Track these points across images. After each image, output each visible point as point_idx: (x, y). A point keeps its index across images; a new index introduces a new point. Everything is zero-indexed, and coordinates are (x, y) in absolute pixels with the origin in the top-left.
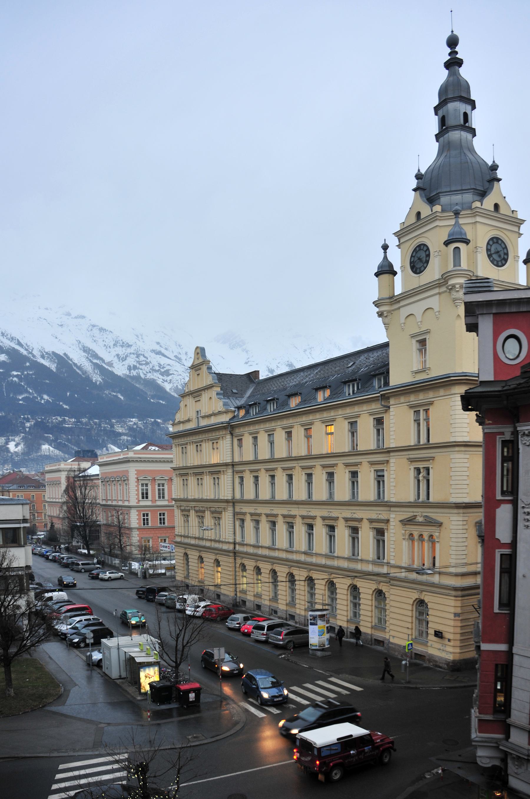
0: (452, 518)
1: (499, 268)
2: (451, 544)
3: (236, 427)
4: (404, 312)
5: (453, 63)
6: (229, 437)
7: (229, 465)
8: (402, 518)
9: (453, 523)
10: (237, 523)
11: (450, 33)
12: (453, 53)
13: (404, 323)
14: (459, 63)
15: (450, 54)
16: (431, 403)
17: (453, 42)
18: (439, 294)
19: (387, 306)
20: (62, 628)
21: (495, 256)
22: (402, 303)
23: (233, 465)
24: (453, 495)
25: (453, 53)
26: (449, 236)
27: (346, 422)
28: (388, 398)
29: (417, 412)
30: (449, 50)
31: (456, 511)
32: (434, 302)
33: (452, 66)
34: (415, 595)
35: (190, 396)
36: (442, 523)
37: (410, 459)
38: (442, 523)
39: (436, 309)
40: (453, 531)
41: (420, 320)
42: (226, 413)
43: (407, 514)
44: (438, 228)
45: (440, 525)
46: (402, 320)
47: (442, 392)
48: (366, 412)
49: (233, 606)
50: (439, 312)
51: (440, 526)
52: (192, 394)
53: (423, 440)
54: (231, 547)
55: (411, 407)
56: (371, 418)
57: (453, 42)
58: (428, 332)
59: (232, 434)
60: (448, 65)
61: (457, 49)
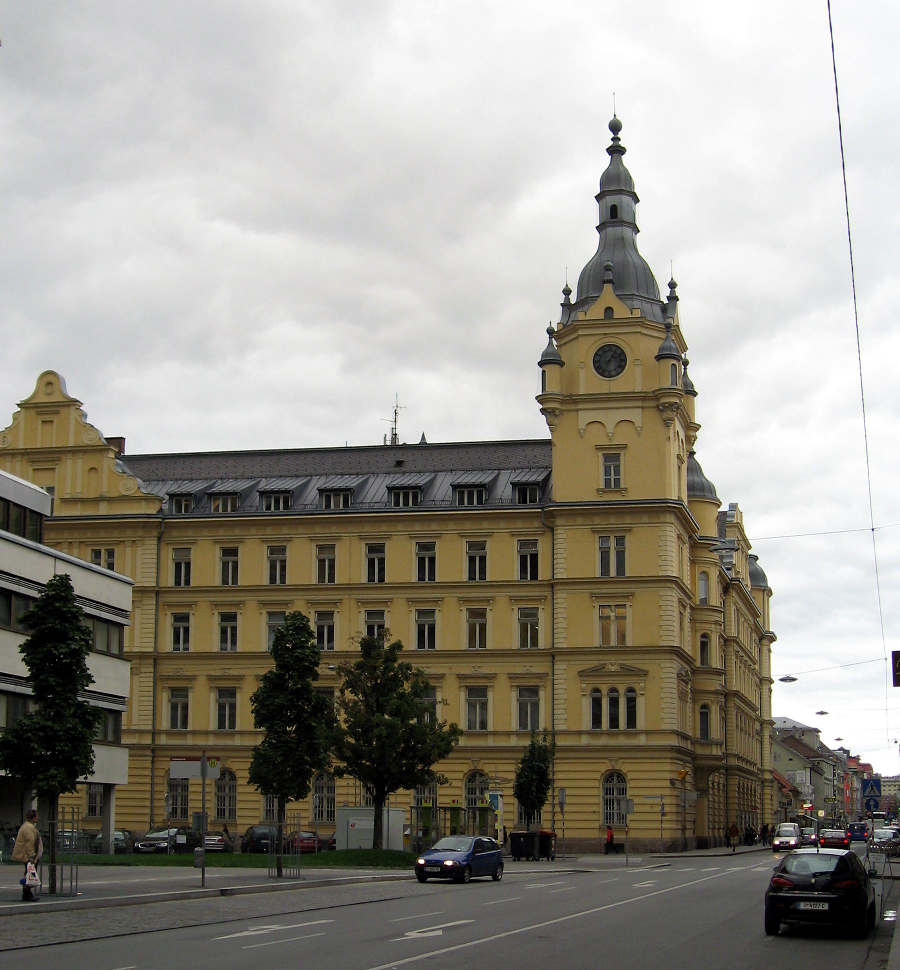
4: (585, 417)
5: (616, 151)
6: (152, 544)
7: (151, 591)
10: (165, 698)
12: (616, 139)
13: (585, 430)
14: (623, 151)
15: (613, 139)
16: (630, 530)
17: (615, 127)
18: (643, 408)
19: (552, 405)
22: (581, 406)
23: (158, 593)
25: (616, 139)
27: (314, 545)
30: (612, 136)
32: (636, 415)
34: (604, 767)
35: (26, 457)
37: (592, 593)
39: (639, 423)
42: (145, 499)
43: (591, 662)
44: (639, 335)
45: (645, 673)
46: (582, 426)
47: (645, 519)
50: (642, 428)
52: (28, 454)
54: (148, 740)
56: (516, 539)
57: (615, 127)
58: (624, 447)
59: (159, 539)
61: (620, 135)
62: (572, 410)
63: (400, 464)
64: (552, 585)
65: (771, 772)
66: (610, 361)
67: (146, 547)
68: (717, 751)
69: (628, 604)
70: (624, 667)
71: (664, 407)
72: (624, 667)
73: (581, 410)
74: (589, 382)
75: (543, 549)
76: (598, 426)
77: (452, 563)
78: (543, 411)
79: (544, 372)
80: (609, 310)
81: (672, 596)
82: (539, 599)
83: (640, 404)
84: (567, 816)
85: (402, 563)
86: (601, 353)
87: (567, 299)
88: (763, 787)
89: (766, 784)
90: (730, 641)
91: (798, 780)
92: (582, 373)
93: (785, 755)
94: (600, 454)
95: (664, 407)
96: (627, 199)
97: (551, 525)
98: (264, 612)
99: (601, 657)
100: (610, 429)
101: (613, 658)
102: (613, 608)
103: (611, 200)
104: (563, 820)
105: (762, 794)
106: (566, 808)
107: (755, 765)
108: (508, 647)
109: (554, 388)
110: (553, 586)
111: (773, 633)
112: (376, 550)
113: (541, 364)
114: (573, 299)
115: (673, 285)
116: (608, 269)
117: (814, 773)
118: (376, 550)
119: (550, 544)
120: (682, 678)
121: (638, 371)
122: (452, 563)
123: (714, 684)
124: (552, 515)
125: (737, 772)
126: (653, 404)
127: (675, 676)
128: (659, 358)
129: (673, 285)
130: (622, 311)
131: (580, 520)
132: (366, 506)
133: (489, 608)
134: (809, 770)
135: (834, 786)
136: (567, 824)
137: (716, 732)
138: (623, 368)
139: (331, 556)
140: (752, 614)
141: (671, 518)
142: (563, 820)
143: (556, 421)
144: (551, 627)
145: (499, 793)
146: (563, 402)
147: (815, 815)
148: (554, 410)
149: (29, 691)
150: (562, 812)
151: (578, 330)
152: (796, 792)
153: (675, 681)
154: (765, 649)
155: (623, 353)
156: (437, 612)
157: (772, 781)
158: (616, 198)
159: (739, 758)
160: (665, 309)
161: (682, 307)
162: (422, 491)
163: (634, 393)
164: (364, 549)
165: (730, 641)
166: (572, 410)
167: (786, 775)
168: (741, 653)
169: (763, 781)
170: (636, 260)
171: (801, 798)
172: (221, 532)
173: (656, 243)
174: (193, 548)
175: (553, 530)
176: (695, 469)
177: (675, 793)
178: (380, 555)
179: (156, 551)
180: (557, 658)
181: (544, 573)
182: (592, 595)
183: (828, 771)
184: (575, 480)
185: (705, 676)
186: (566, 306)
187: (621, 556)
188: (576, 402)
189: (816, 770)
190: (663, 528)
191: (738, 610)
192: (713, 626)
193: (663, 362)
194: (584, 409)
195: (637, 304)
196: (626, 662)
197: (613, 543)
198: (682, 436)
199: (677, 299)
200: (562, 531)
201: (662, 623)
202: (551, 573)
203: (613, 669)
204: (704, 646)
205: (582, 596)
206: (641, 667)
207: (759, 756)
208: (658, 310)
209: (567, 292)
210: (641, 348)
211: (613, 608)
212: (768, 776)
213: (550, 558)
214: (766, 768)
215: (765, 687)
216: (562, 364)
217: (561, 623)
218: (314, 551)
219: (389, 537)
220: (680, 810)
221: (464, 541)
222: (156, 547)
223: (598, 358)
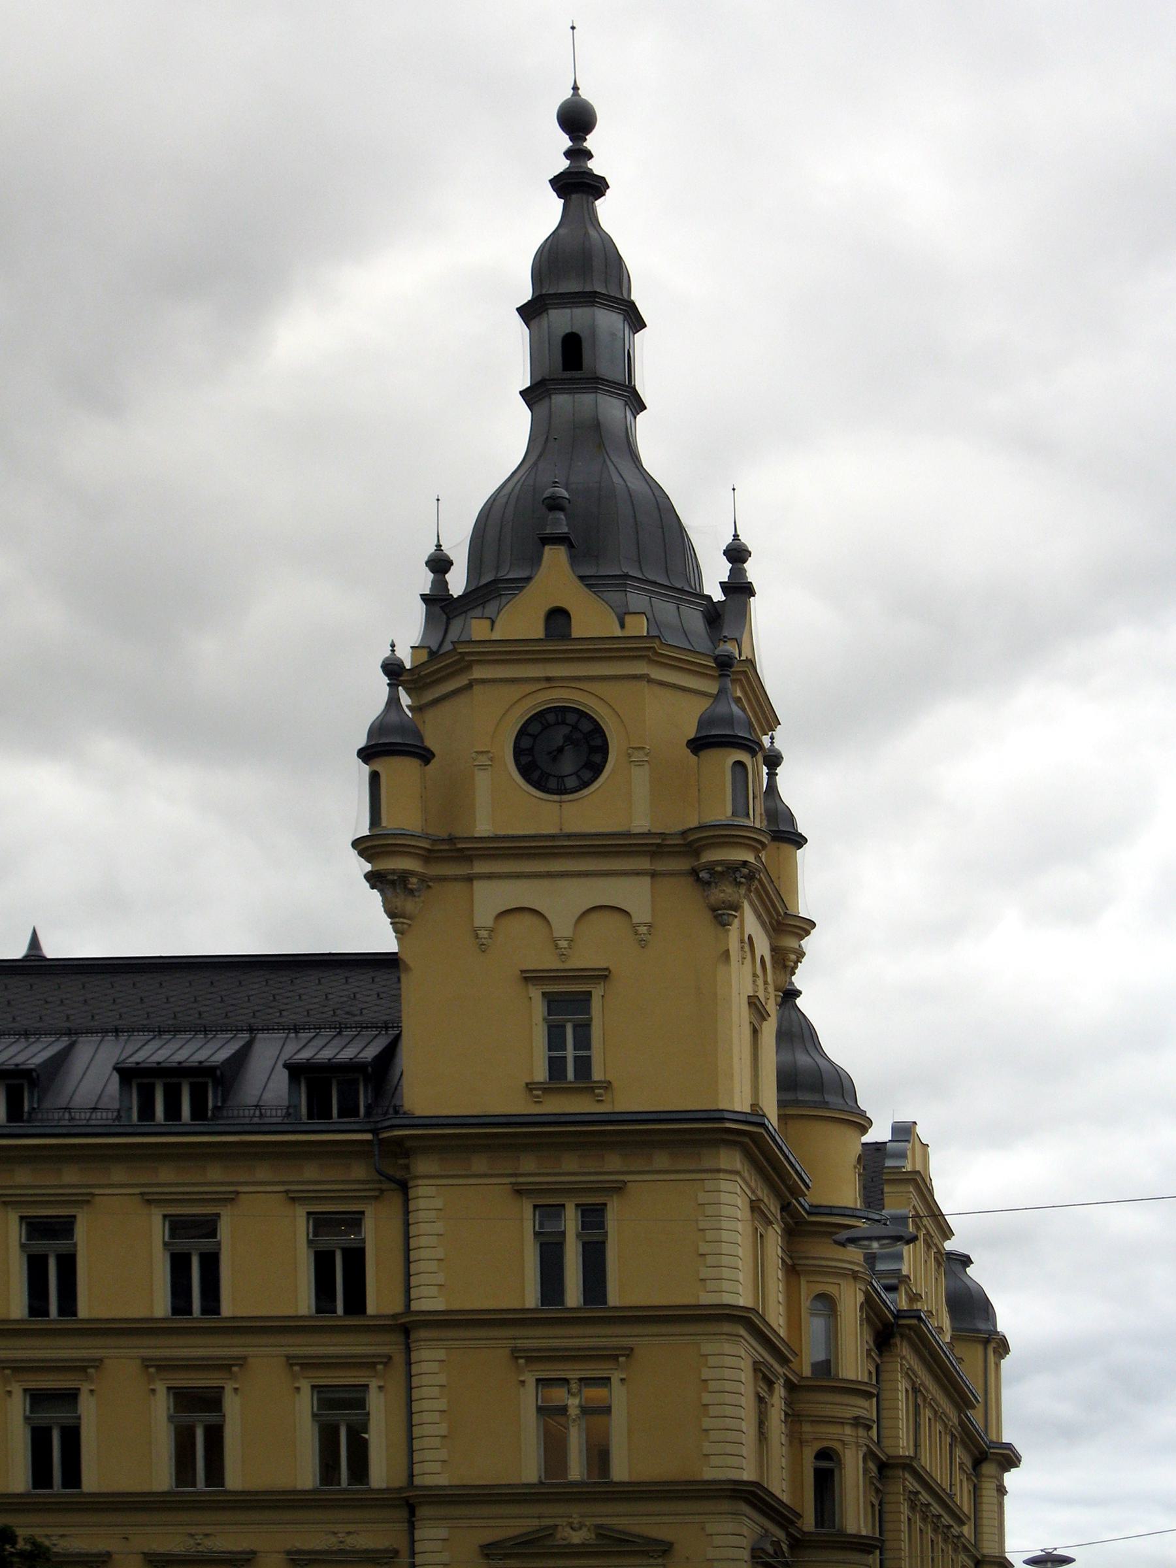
0: (710, 1528)
1: (596, 785)
4: (490, 897)
5: (579, 186)
8: (488, 1536)
9: (717, 1540)
11: (568, 94)
12: (578, 154)
13: (491, 930)
14: (598, 187)
15: (568, 154)
16: (619, 1189)
17: (577, 120)
18: (654, 875)
21: (483, 723)
22: (480, 867)
24: (715, 1461)
25: (578, 154)
26: (701, 724)
28: (407, 1154)
29: (549, 1212)
30: (566, 142)
31: (726, 1506)
32: (634, 894)
33: (583, 192)
36: (671, 1545)
38: (671, 1545)
39: (641, 912)
41: (568, 933)
46: (484, 917)
47: (662, 1160)
48: (137, 1191)
50: (650, 926)
51: (665, 1552)
55: (520, 1192)
57: (577, 120)
58: (602, 976)
60: (564, 185)
61: (591, 142)
62: (455, 879)
64: (407, 1327)
66: (560, 749)
69: (616, 1377)
70: (602, 1533)
71: (712, 872)
72: (602, 1533)
74: (501, 802)
75: (377, 1234)
76: (528, 920)
78: (374, 879)
79: (375, 778)
80: (558, 617)
82: (368, 1364)
83: (644, 864)
87: (440, 583)
92: (482, 781)
94: (536, 993)
95: (712, 872)
97: (399, 1175)
100: (563, 927)
101: (575, 1511)
102: (574, 1387)
103: (561, 320)
109: (404, 817)
111: (1009, 1446)
113: (366, 754)
114: (457, 582)
115: (737, 554)
119: (397, 1224)
121: (640, 778)
124: (400, 1150)
126: (683, 864)
128: (698, 745)
129: (737, 554)
130: (592, 619)
131: (480, 1164)
141: (731, 1159)
143: (410, 906)
146: (429, 856)
154: (988, 1488)
160: (714, 615)
161: (763, 612)
163: (628, 835)
166: (455, 879)
168: (925, 1497)
170: (635, 484)
175: (404, 1187)
176: (798, 1033)
181: (380, 1297)
182: (516, 1354)
184: (465, 1058)
192: (848, 1430)
194: (490, 876)
197: (571, 1223)
198: (763, 947)
200: (431, 1191)
208: (695, 620)
209: (439, 564)
210: (650, 717)
211: (574, 1387)
216: (425, 756)
217: (431, 1425)
223: (526, 743)
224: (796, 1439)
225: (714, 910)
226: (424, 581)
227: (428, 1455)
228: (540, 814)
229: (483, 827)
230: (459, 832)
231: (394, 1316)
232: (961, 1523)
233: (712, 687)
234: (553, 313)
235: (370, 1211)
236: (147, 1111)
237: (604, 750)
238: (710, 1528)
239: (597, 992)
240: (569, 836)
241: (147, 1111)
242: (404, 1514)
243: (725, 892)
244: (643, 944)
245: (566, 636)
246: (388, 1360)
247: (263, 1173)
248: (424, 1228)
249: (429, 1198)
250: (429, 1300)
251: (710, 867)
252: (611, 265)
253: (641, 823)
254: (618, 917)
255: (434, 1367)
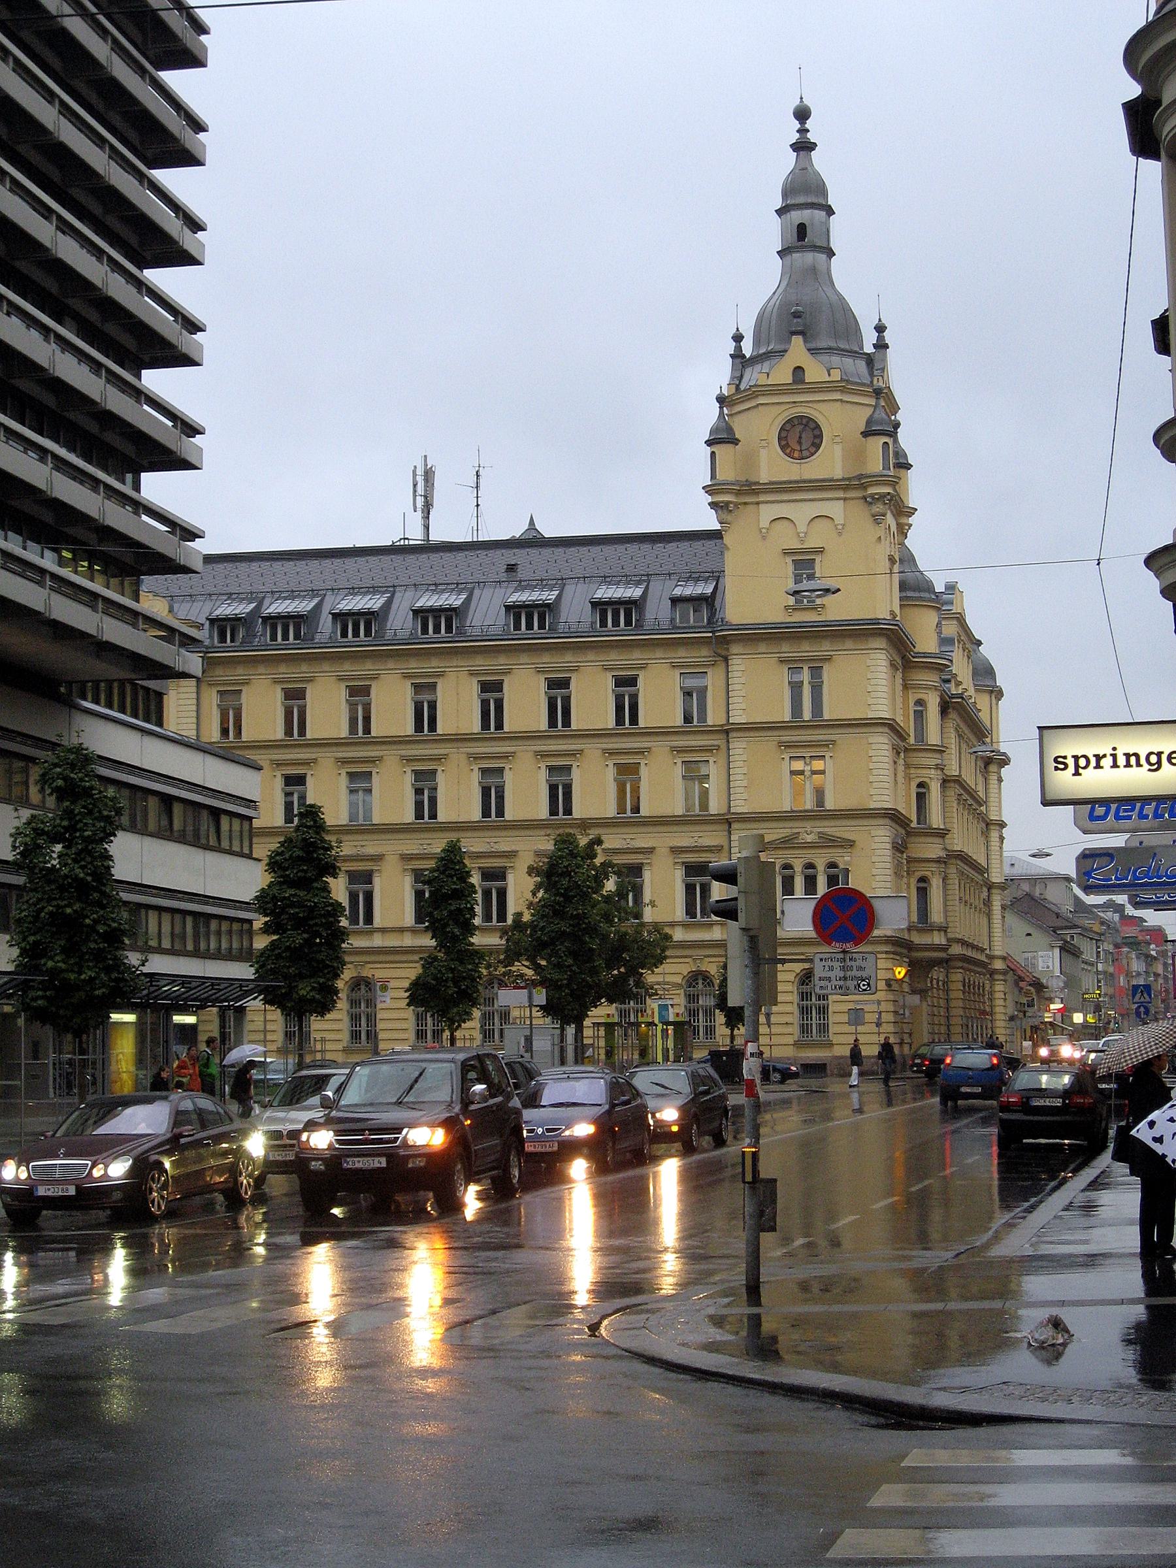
0: (873, 833)
2: (875, 872)
3: (735, 641)
4: (767, 513)
5: (803, 147)
11: (798, 102)
12: (803, 131)
14: (811, 147)
16: (828, 659)
17: (802, 114)
18: (845, 499)
20: (125, 1042)
22: (762, 498)
25: (803, 131)
32: (835, 509)
39: (839, 520)
40: (878, 852)
45: (850, 844)
47: (849, 644)
49: (623, 943)
53: (807, 715)
57: (802, 114)
58: (820, 551)
61: (809, 124)
62: (752, 503)
63: (511, 568)
64: (727, 731)
65: (1004, 958)
66: (801, 436)
67: (182, 690)
68: (938, 939)
69: (828, 755)
70: (821, 835)
71: (873, 498)
72: (821, 835)
73: (763, 502)
74: (773, 465)
75: (713, 680)
76: (786, 523)
77: (593, 703)
78: (713, 505)
79: (713, 453)
80: (798, 371)
81: (881, 744)
82: (708, 750)
83: (841, 494)
84: (774, 1030)
85: (526, 704)
86: (788, 427)
87: (738, 348)
88: (992, 980)
89: (996, 977)
90: (949, 781)
91: (1041, 965)
92: (763, 454)
93: (1018, 926)
94: (789, 560)
95: (873, 498)
96: (821, 214)
97: (724, 653)
98: (343, 772)
99: (791, 824)
100: (802, 528)
101: (808, 825)
102: (808, 760)
103: (797, 216)
104: (770, 1034)
105: (991, 993)
106: (773, 1019)
107: (983, 950)
108: (668, 811)
109: (726, 474)
110: (727, 732)
111: (1004, 754)
112: (491, 688)
113: (709, 443)
114: (748, 349)
115: (880, 329)
116: (797, 315)
117: (1064, 954)
118: (491, 688)
119: (723, 676)
120: (899, 848)
121: (838, 450)
122: (593, 703)
123: (932, 849)
124: (725, 641)
125: (960, 964)
126: (859, 494)
127: (889, 846)
128: (866, 434)
129: (880, 329)
130: (815, 372)
131: (762, 647)
132: (477, 632)
133: (643, 762)
134: (1057, 951)
135: (1098, 973)
136: (775, 1040)
137: (936, 916)
138: (818, 447)
139: (430, 697)
140: (975, 734)
141: (881, 643)
142: (770, 1034)
143: (729, 518)
144: (725, 786)
145: (669, 1002)
146: (739, 493)
147: (1067, 1020)
148: (727, 503)
149: (20, 880)
150: (769, 1024)
151: (757, 396)
152: (1039, 986)
153: (889, 853)
154: (993, 778)
155: (818, 427)
156: (574, 769)
157: (1005, 973)
158: (805, 218)
159: (963, 943)
160: (869, 360)
161: (894, 359)
162: (551, 610)
163: (831, 480)
164: (475, 688)
165: (949, 781)
166: (752, 503)
167: (1020, 958)
168: (965, 796)
169: (993, 973)
170: (834, 298)
171: (1047, 995)
172: (283, 668)
173: (859, 278)
174: (245, 689)
175: (726, 659)
176: (907, 559)
177: (891, 997)
178: (497, 695)
179: (194, 695)
180: (734, 826)
181: (714, 717)
182: (780, 744)
183: (1088, 951)
184: (754, 593)
185: (922, 839)
186: (737, 356)
187: (817, 690)
188: (756, 493)
189: (1069, 950)
190: (872, 656)
191: (960, 736)
192: (933, 771)
193: (870, 439)
194: (767, 502)
195: (836, 360)
196: (826, 830)
197: (805, 676)
198: (894, 528)
199: (886, 346)
200: (739, 661)
201: (872, 779)
202: (724, 715)
203: (809, 838)
204: (921, 798)
205: (767, 745)
206: (846, 836)
207: (986, 939)
208: (862, 365)
209: (738, 338)
210: (840, 420)
211: (808, 760)
212: (998, 965)
213: (724, 694)
214: (997, 953)
215: (994, 835)
216: (735, 442)
217: (738, 781)
218: (409, 691)
219: (508, 672)
220: (898, 1018)
221: (609, 675)
222: (194, 689)
223: (784, 434)
224: (908, 778)
225: (873, 516)
226: (731, 347)
227: (738, 796)
228: (790, 470)
229: (764, 478)
230: (753, 479)
231: (722, 726)
232: (981, 805)
233: (873, 402)
234: (793, 213)
235: (710, 671)
236: (603, 623)
237: (821, 436)
238: (873, 833)
239: (818, 559)
240: (805, 481)
241: (603, 623)
242: (726, 827)
243: (878, 508)
244: (840, 534)
245: (803, 382)
246: (718, 748)
247: (659, 653)
248: (736, 680)
249: (737, 664)
250: (738, 718)
251: (872, 496)
252: (821, 189)
253: (838, 473)
254: (826, 520)
255: (740, 751)
